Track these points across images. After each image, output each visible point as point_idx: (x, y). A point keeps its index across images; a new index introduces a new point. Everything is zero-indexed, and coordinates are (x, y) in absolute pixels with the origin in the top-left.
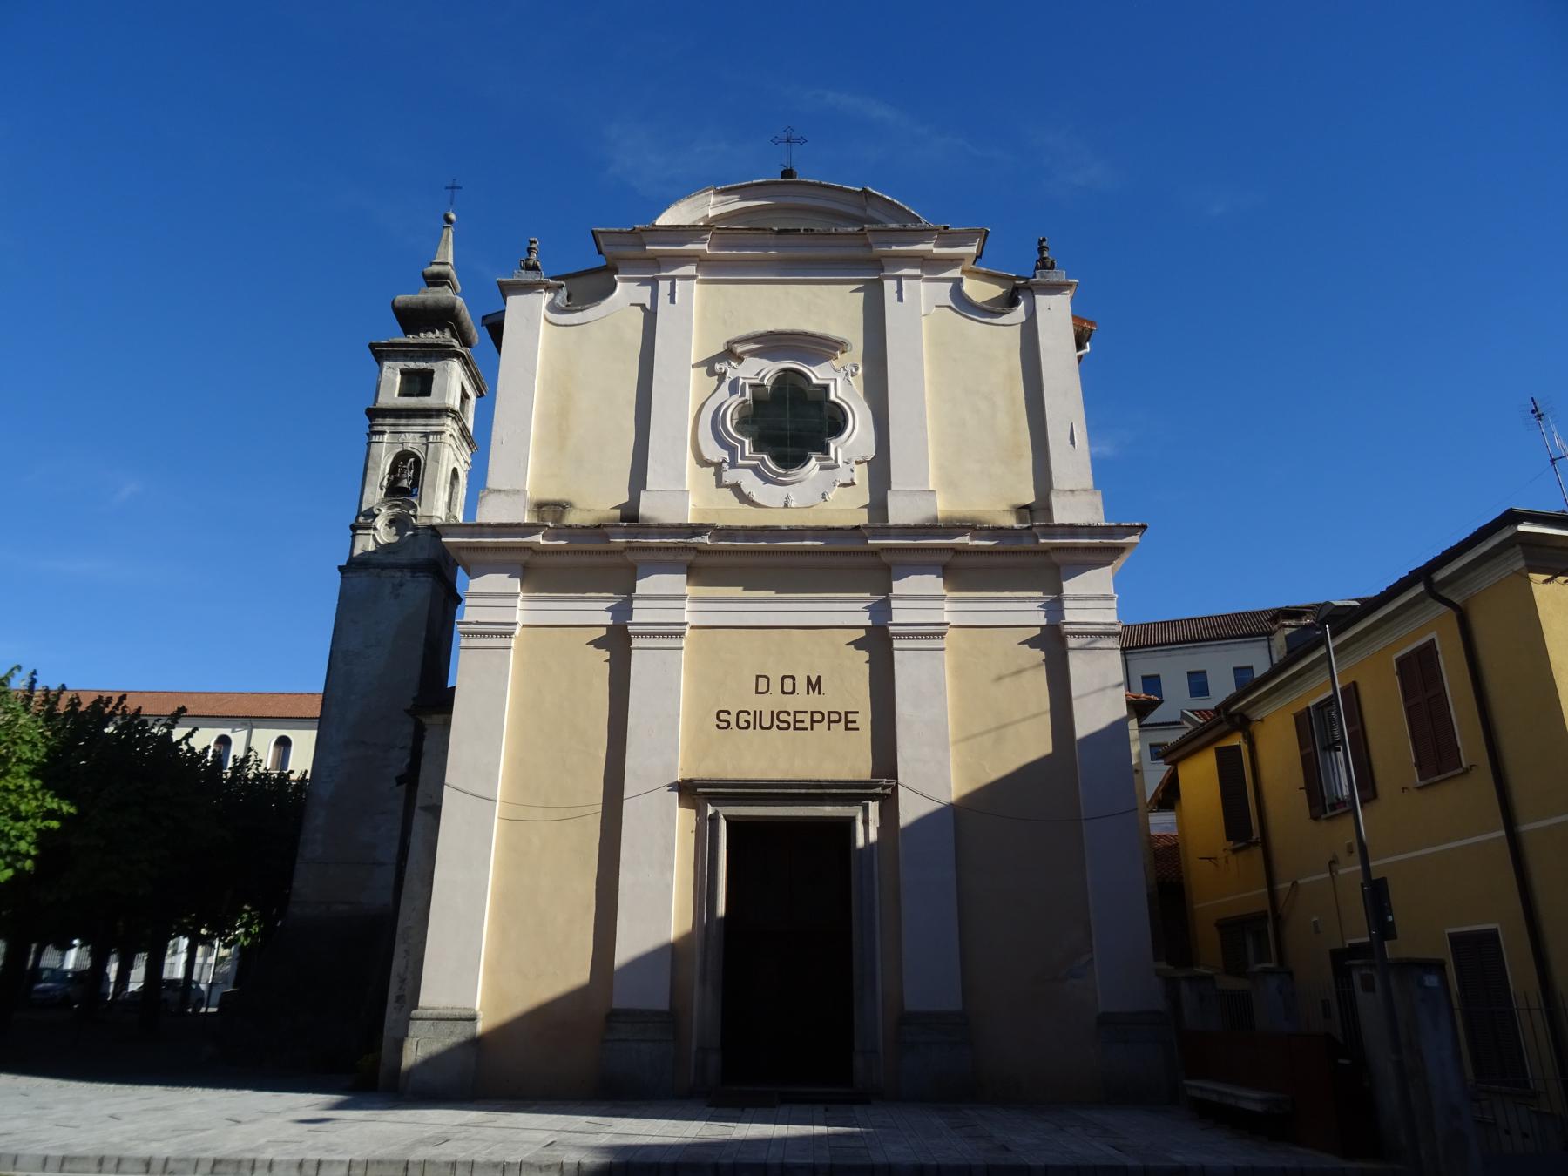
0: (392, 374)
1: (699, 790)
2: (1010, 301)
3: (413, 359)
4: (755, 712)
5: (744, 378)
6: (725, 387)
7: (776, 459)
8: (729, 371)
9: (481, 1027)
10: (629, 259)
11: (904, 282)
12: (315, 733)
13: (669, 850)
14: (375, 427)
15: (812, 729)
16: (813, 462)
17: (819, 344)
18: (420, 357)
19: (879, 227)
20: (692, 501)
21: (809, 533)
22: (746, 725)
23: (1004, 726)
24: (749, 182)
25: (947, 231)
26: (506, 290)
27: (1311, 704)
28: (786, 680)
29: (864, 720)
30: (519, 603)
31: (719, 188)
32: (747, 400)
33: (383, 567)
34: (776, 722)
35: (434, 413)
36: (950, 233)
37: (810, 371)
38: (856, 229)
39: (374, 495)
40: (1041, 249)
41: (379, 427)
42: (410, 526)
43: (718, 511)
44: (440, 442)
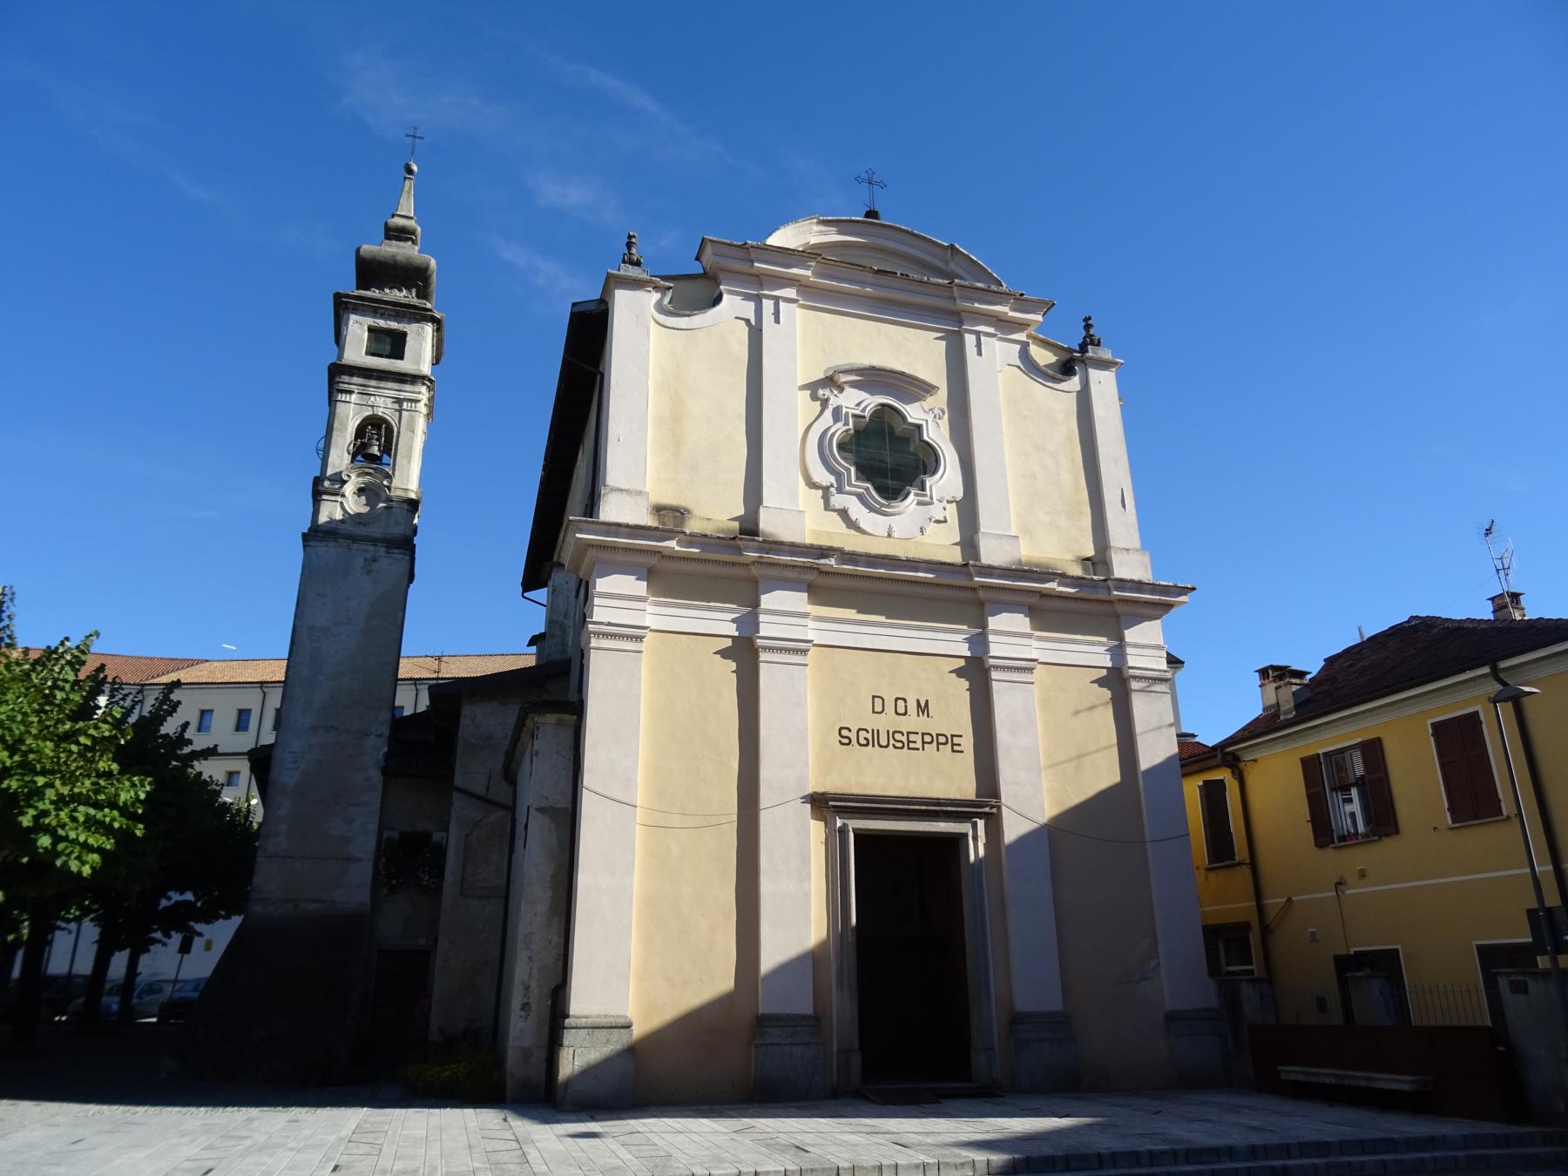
0: (358, 329)
1: (831, 803)
3: (382, 316)
4: (873, 730)
5: (846, 407)
6: (828, 413)
7: (879, 490)
8: (832, 397)
9: (638, 1030)
10: (733, 272)
11: (782, 304)
13: (805, 859)
14: (341, 385)
15: (923, 749)
16: (912, 497)
17: (913, 385)
21: (923, 565)
22: (865, 742)
23: (1082, 756)
24: (848, 218)
25: (1021, 297)
27: (1320, 751)
28: (899, 701)
29: (967, 743)
32: (850, 429)
33: (355, 539)
34: (892, 741)
35: (409, 379)
36: (1023, 300)
38: (946, 282)
39: (340, 459)
40: (629, 245)
41: (346, 386)
42: (383, 498)
43: (829, 534)
44: (416, 411)
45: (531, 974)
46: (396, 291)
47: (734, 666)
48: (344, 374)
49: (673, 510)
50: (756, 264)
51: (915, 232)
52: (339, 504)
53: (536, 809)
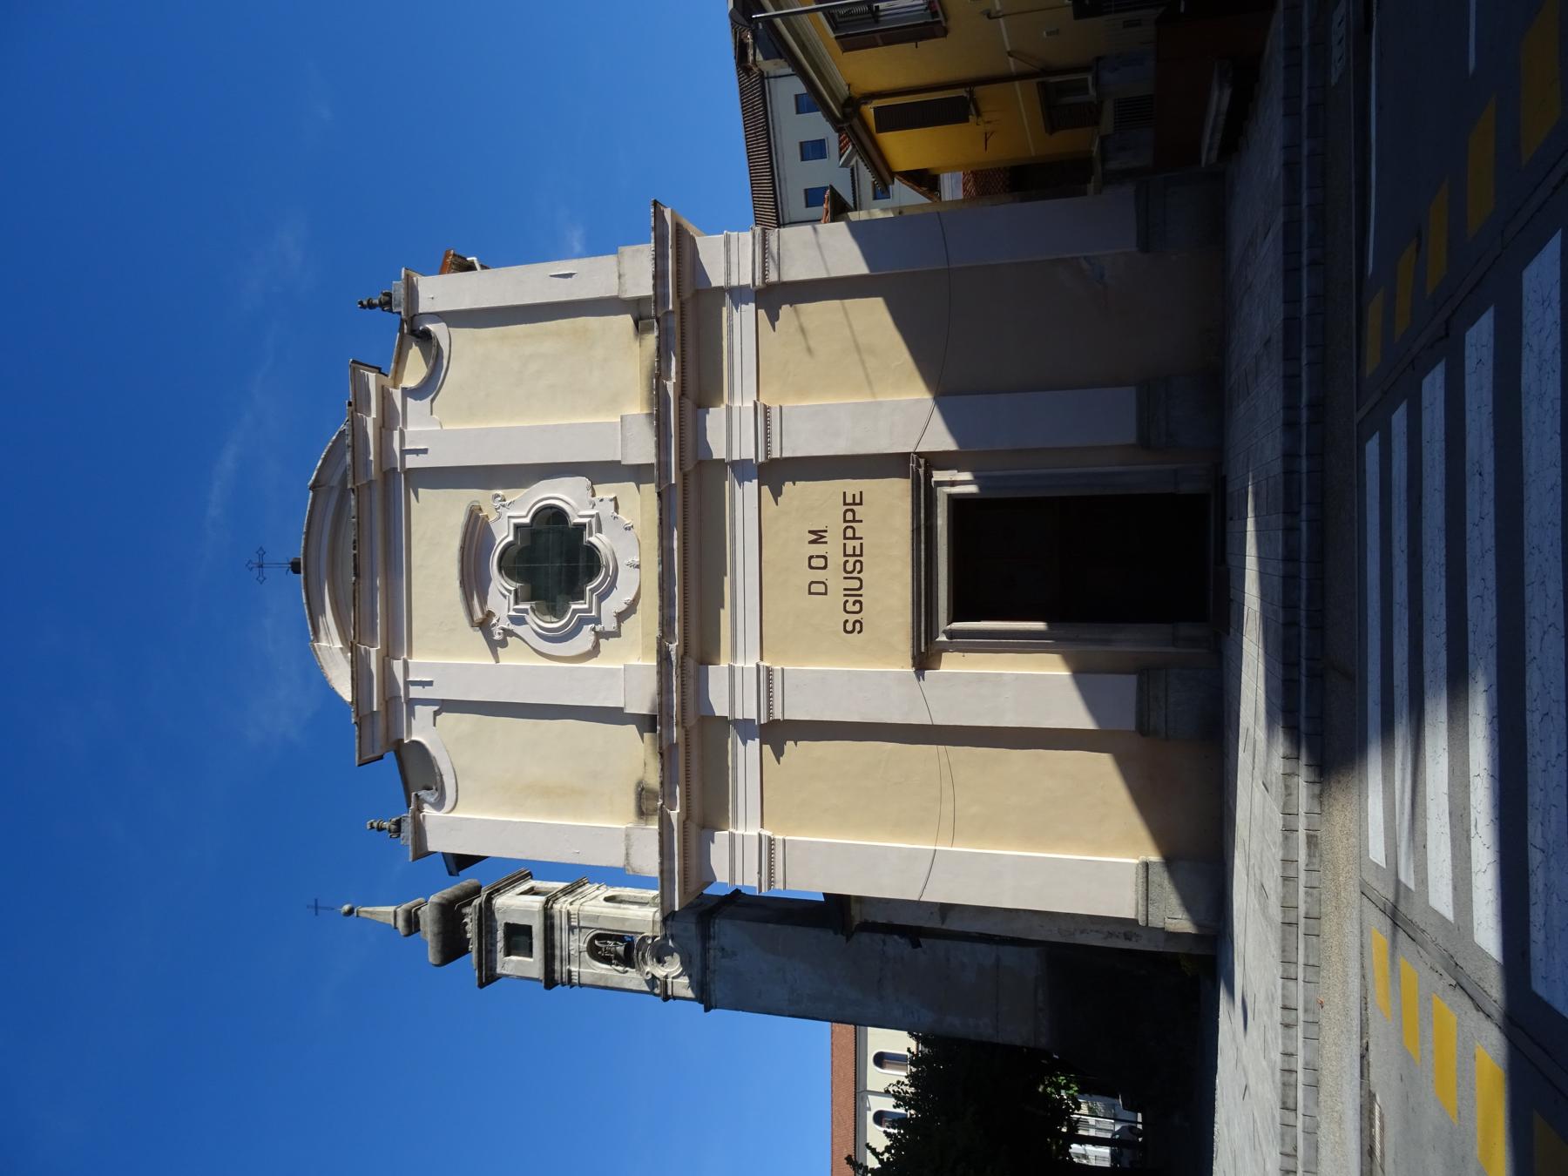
0: (510, 965)
1: (923, 649)
2: (425, 338)
3: (494, 944)
4: (845, 595)
5: (509, 610)
6: (518, 629)
8: (502, 625)
9: (1154, 857)
12: (869, 1028)
13: (981, 678)
14: (564, 980)
15: (861, 538)
16: (593, 540)
17: (473, 533)
18: (491, 937)
19: (350, 474)
20: (634, 661)
21: (665, 543)
22: (858, 605)
24: (306, 607)
25: (353, 404)
26: (421, 852)
27: (832, 35)
28: (813, 564)
29: (852, 486)
30: (739, 832)
31: (312, 637)
33: (705, 968)
34: (855, 574)
35: (549, 922)
37: (499, 544)
38: (352, 496)
39: (633, 979)
40: (371, 306)
41: (564, 976)
42: (663, 942)
43: (645, 635)
45: (1097, 931)
46: (467, 927)
47: (790, 744)
48: (554, 977)
49: (640, 799)
50: (375, 709)
51: (305, 530)
52: (674, 980)
53: (943, 923)
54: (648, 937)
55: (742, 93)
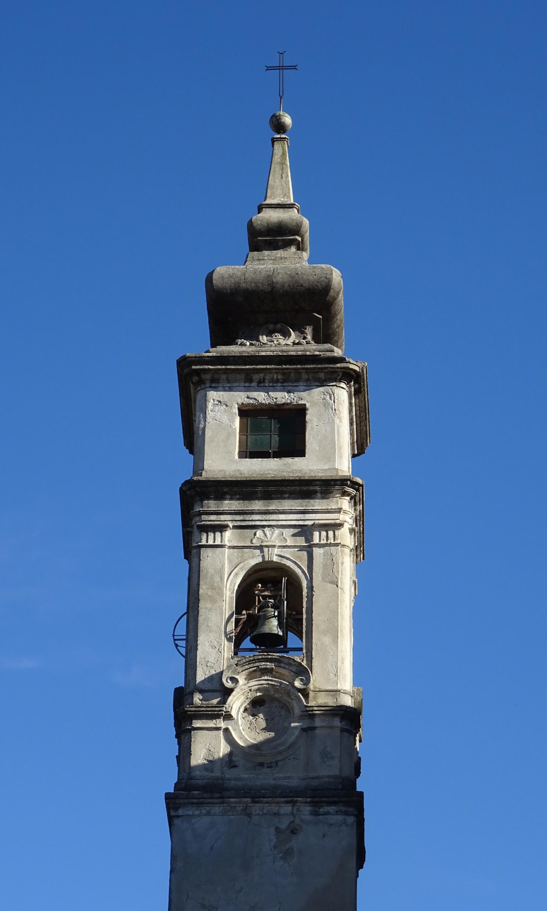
3: (261, 386)
14: (204, 517)
18: (277, 381)
41: (213, 517)
42: (297, 711)
44: (337, 545)
48: (209, 499)
54: (307, 682)
55: (171, 860)
